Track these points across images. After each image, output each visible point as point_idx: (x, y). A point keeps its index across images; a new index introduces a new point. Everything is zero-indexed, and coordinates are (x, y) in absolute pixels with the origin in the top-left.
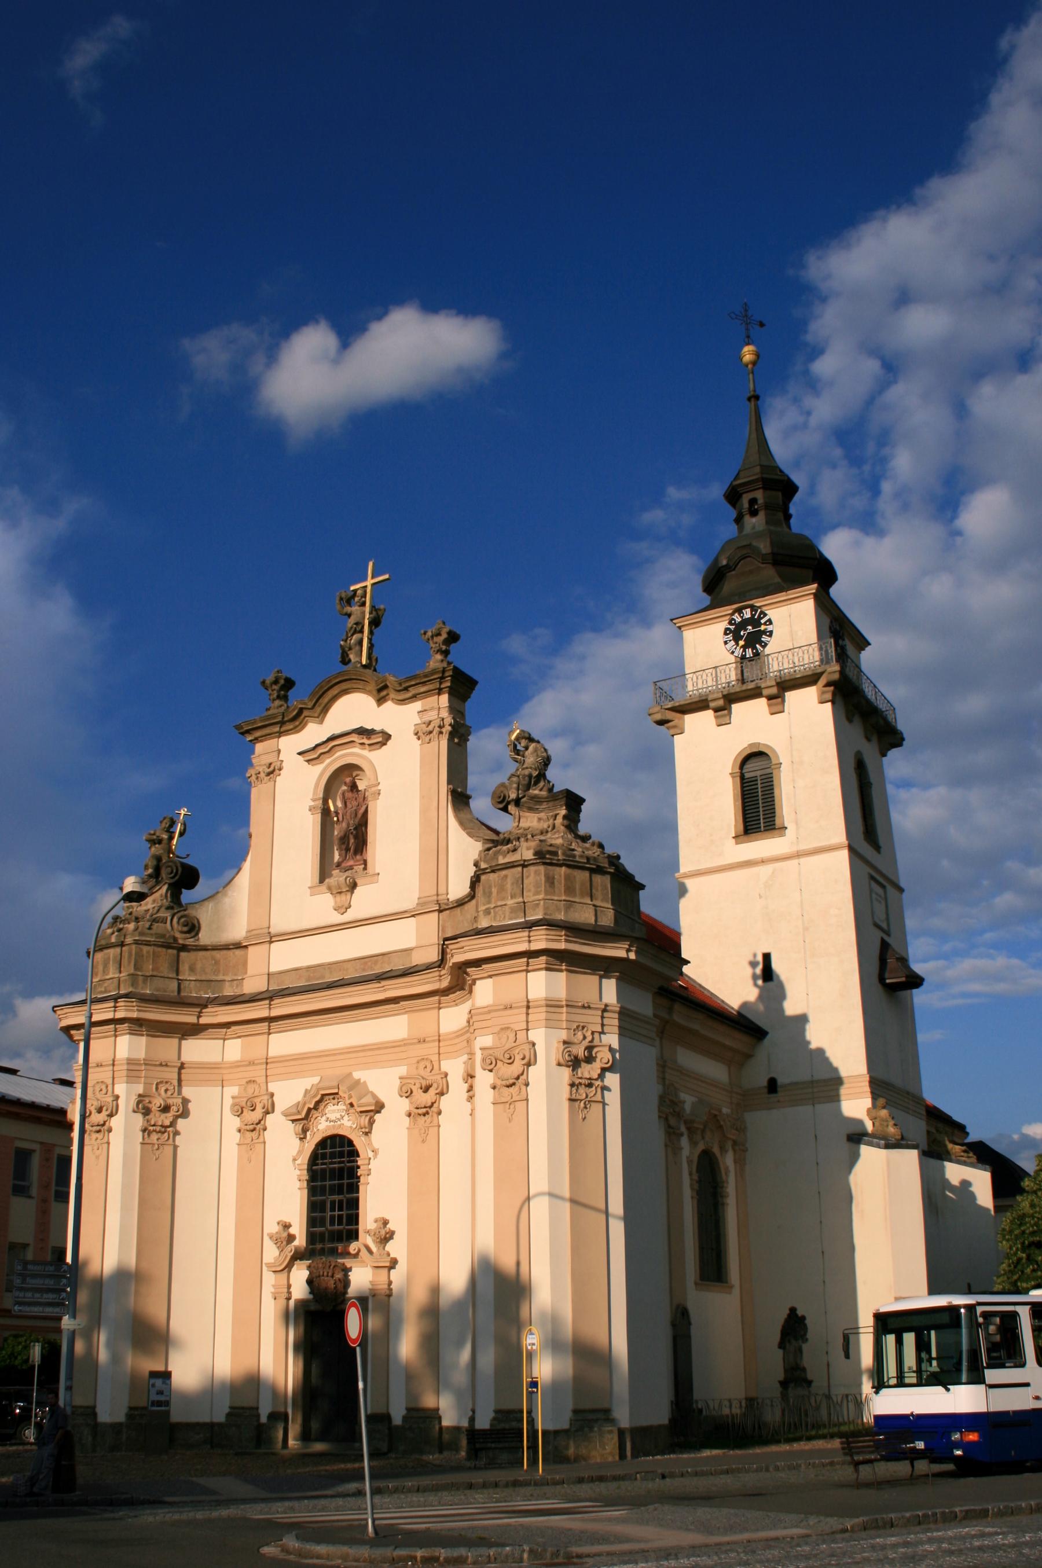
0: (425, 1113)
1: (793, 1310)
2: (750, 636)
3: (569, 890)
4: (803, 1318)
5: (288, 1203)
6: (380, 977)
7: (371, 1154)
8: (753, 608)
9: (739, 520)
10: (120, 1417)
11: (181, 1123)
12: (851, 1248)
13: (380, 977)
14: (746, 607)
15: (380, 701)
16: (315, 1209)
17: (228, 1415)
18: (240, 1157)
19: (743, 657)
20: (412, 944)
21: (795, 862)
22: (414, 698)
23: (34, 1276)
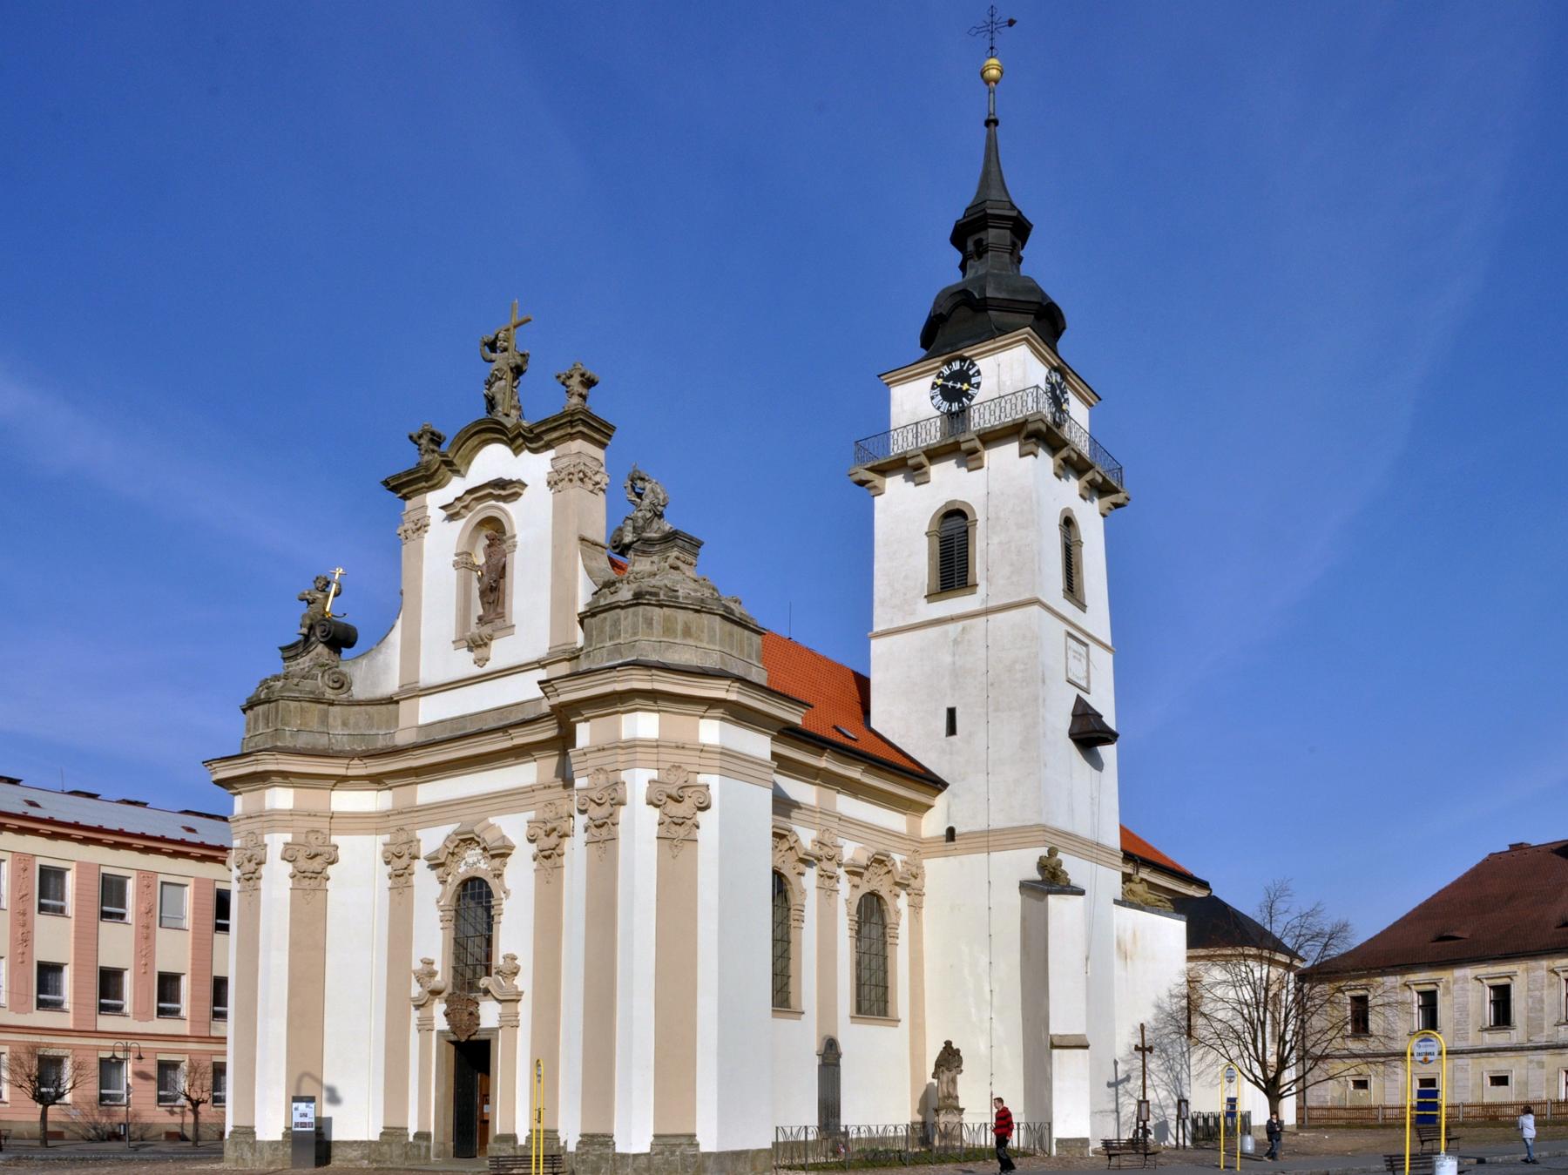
0: (549, 856)
1: (948, 1044)
2: (955, 391)
5: (432, 942)
6: (504, 729)
8: (963, 359)
10: (277, 1136)
11: (331, 870)
13: (504, 729)
14: (954, 359)
15: (517, 451)
16: (459, 946)
18: (392, 901)
21: (983, 619)
22: (549, 446)
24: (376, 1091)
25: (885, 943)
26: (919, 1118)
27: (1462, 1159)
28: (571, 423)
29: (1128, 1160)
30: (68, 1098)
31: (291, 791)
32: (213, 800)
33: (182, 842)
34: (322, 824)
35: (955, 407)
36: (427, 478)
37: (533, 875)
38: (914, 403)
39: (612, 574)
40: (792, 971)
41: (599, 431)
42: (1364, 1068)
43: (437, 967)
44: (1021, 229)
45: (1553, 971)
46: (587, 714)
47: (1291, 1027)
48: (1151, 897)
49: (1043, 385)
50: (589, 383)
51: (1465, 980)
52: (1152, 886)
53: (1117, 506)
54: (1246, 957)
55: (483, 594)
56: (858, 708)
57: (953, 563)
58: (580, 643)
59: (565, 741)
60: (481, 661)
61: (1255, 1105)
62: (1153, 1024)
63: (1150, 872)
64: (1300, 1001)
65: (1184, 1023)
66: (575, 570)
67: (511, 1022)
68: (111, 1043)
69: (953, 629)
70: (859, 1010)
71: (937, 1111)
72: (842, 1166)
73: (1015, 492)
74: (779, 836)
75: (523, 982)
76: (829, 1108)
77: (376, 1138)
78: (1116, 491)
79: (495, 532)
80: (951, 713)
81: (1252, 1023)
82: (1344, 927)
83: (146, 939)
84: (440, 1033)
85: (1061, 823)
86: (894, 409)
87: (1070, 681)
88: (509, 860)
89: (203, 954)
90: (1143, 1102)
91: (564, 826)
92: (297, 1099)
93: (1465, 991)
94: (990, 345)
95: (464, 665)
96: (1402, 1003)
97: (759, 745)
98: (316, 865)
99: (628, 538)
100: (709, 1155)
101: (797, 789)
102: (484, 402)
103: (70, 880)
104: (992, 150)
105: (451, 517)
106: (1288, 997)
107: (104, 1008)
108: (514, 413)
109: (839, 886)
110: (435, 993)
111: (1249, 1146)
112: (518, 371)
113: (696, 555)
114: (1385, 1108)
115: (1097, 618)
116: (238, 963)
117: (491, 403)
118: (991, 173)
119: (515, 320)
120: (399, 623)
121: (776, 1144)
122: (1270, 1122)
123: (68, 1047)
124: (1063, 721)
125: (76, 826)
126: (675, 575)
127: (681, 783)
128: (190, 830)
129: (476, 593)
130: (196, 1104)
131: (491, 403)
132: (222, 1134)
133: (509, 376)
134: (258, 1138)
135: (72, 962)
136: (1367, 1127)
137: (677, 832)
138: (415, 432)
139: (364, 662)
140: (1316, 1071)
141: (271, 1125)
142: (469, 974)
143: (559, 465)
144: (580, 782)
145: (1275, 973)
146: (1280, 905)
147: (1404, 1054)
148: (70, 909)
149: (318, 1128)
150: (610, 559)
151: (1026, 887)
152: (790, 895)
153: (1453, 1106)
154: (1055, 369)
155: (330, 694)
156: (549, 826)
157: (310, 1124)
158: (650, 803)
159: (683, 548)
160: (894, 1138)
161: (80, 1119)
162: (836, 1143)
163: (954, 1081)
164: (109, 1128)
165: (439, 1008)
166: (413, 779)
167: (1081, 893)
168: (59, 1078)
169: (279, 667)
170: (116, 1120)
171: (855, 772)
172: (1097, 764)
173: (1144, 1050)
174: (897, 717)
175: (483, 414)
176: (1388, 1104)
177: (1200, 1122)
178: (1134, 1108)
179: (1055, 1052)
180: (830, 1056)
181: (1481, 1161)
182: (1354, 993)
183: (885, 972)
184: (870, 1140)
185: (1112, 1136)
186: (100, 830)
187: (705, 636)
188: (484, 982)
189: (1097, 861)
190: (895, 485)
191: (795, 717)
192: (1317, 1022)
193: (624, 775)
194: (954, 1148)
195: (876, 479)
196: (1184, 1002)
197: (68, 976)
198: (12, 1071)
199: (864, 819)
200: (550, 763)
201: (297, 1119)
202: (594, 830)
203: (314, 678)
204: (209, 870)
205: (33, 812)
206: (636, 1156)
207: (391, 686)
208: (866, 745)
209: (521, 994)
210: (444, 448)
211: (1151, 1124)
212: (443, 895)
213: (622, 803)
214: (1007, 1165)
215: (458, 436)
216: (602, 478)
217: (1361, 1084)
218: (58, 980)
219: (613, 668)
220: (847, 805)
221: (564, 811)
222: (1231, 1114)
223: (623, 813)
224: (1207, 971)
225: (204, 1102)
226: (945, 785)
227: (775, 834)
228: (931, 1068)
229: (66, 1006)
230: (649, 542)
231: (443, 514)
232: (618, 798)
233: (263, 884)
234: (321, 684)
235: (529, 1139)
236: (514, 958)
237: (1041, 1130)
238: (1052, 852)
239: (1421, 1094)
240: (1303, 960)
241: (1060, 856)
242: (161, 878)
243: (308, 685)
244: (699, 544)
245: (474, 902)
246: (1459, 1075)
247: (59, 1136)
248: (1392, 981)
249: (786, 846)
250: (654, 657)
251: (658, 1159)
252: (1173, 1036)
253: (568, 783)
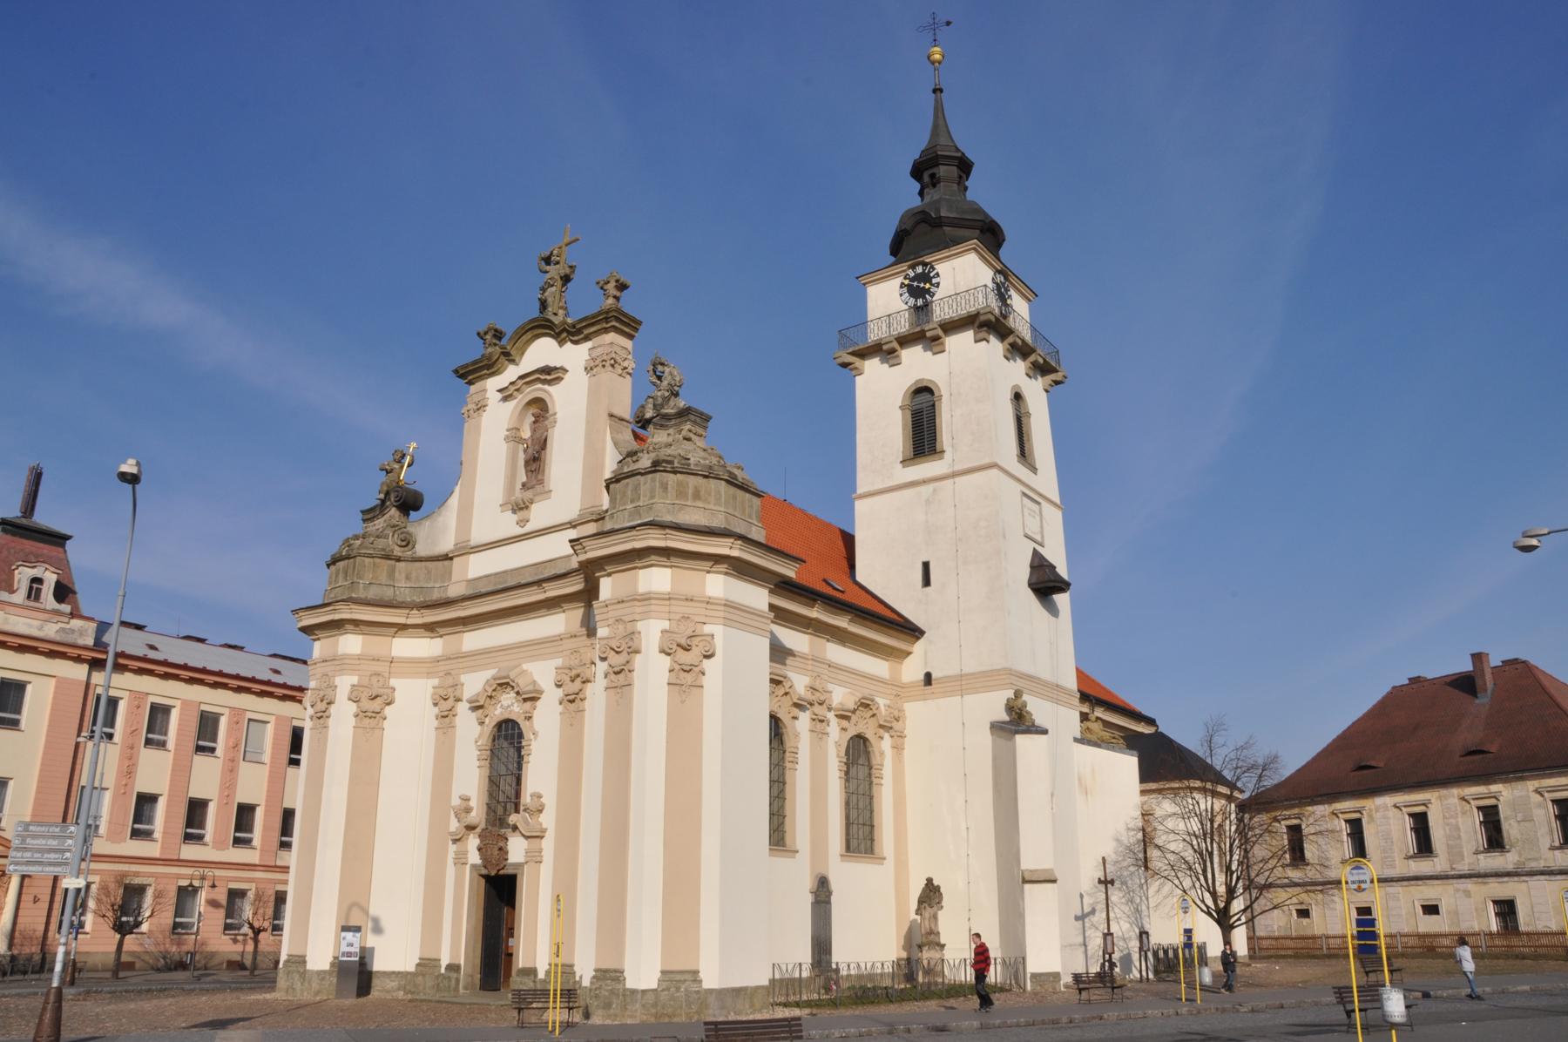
1: (930, 881)
2: (920, 289)
5: (470, 780)
6: (539, 583)
8: (925, 264)
11: (388, 710)
13: (539, 583)
16: (493, 782)
21: (950, 481)
22: (587, 338)
23: (35, 837)
24: (414, 926)
25: (871, 783)
26: (904, 955)
27: (1407, 991)
28: (607, 320)
29: (1097, 994)
30: (144, 927)
31: (360, 637)
32: (296, 645)
33: (269, 683)
34: (382, 668)
35: (920, 302)
36: (488, 367)
37: (558, 717)
38: (886, 300)
39: (634, 445)
40: (788, 811)
41: (627, 325)
42: (1304, 896)
43: (473, 803)
44: (965, 166)
45: (1463, 799)
46: (610, 569)
47: (1236, 857)
48: (1106, 735)
49: (991, 285)
50: (622, 287)
51: (1386, 807)
52: (1107, 724)
53: (1057, 383)
54: (1192, 789)
55: (527, 463)
56: (845, 564)
57: (923, 436)
58: (606, 506)
59: (589, 594)
60: (522, 522)
61: (1209, 935)
62: (1114, 857)
63: (1106, 711)
64: (1242, 831)
65: (1141, 855)
66: (604, 441)
67: (535, 858)
68: (189, 871)
69: (926, 490)
70: (848, 848)
71: (920, 947)
72: (834, 1004)
73: (973, 373)
74: (775, 682)
75: (547, 820)
76: (821, 947)
78: (1055, 371)
79: (540, 408)
80: (926, 566)
81: (1201, 854)
82: (1274, 759)
83: (231, 770)
84: (474, 866)
85: (1025, 667)
86: (871, 304)
87: (1027, 536)
88: (538, 703)
89: (277, 785)
90: (1108, 935)
91: (587, 674)
92: (345, 929)
93: (1386, 817)
94: (946, 253)
95: (508, 524)
96: (1332, 831)
97: (758, 597)
98: (376, 705)
99: (649, 415)
100: (711, 991)
101: (793, 639)
102: (538, 304)
103: (174, 716)
104: (939, 110)
105: (505, 399)
106: (1231, 828)
107: (188, 837)
108: (561, 312)
109: (829, 730)
110: (470, 828)
111: (1206, 976)
112: (566, 279)
113: (705, 428)
114: (1328, 937)
115: (1047, 479)
116: (305, 796)
117: (544, 305)
118: (939, 124)
119: (567, 240)
120: (457, 490)
121: (773, 981)
122: (1224, 952)
123: (151, 875)
124: (1021, 572)
125: (185, 667)
126: (688, 445)
127: (689, 632)
128: (276, 672)
129: (521, 463)
130: (257, 932)
131: (544, 305)
132: (277, 962)
133: (559, 283)
134: (309, 966)
135: (166, 793)
136: (1314, 957)
137: (685, 679)
138: (482, 330)
139: (427, 523)
140: (1262, 901)
141: (320, 958)
142: (500, 811)
144: (602, 632)
145: (1219, 804)
146: (1218, 740)
147: (1339, 882)
148: (171, 745)
149: (362, 958)
150: (634, 432)
151: (996, 727)
152: (785, 738)
153: (1392, 936)
154: (999, 272)
155: (398, 552)
156: (574, 673)
157: (354, 954)
158: (662, 651)
159: (695, 422)
160: (882, 975)
161: (152, 949)
162: (828, 979)
163: (935, 917)
164: (177, 958)
165: (473, 842)
166: (460, 628)
167: (1045, 732)
168: (140, 907)
169: (358, 527)
170: (185, 948)
171: (842, 622)
172: (1053, 610)
173: (1106, 882)
174: (881, 571)
175: (536, 314)
176: (1330, 933)
177: (1161, 954)
178: (1100, 941)
179: (1027, 886)
180: (822, 893)
181: (1426, 995)
182: (1289, 822)
183: (872, 812)
184: (860, 977)
185: (1081, 970)
186: (204, 671)
187: (712, 499)
188: (513, 819)
189: (1057, 701)
190: (872, 366)
191: (789, 571)
192: (1259, 852)
193: (640, 626)
194: (936, 984)
195: (857, 361)
196: (1140, 836)
197: (161, 807)
198: (99, 901)
199: (845, 667)
200: (575, 614)
201: (344, 949)
202: (613, 677)
203: (386, 537)
204: (288, 709)
205: (152, 655)
206: (644, 992)
207: (446, 544)
208: (852, 596)
209: (544, 831)
210: (504, 341)
211: (1116, 957)
213: (638, 652)
214: (986, 1001)
215: (516, 332)
216: (630, 364)
217: (1304, 913)
218: (152, 810)
219: (633, 528)
220: (837, 653)
221: (587, 656)
222: (1188, 945)
223: (638, 660)
224: (1159, 804)
225: (265, 930)
226: (922, 633)
227: (772, 681)
228: (914, 905)
229: (157, 835)
230: (667, 417)
231: (500, 396)
232: (634, 645)
233: (331, 722)
234: (391, 543)
235: (548, 973)
236: (540, 797)
237: (1016, 965)
238: (1018, 694)
239: (1360, 923)
240: (1242, 791)
241: (1025, 697)
242: (250, 715)
243: (381, 543)
244: (707, 419)
245: (508, 740)
246: (1391, 903)
247: (130, 966)
248: (1321, 810)
249: (782, 691)
250: (668, 518)
251: (664, 996)
252: (1132, 869)
253: (591, 632)
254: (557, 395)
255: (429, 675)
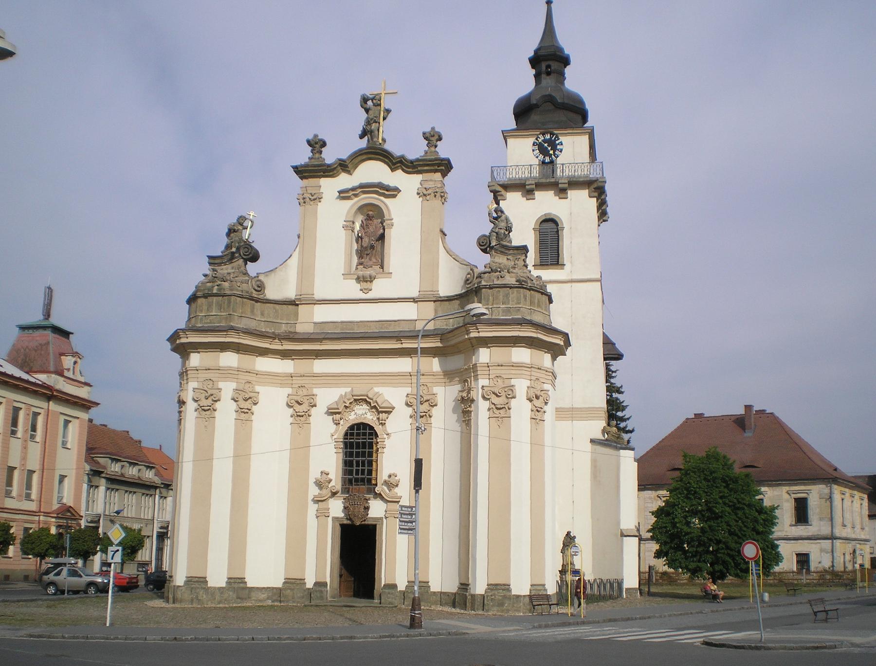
1: (569, 533)
2: (548, 150)
3: (532, 303)
4: (575, 537)
5: (328, 460)
7: (385, 436)
8: (552, 134)
9: (537, 76)
12: (460, 518)
17: (284, 583)
19: (543, 162)
20: (416, 318)
21: (569, 284)
43: (332, 476)
77: (280, 585)
84: (335, 519)
134: (211, 584)
143: (427, 185)
155: (255, 294)
179: (625, 538)
207: (290, 293)
212: (336, 431)
213: (514, 397)
254: (392, 207)
255: (282, 385)
